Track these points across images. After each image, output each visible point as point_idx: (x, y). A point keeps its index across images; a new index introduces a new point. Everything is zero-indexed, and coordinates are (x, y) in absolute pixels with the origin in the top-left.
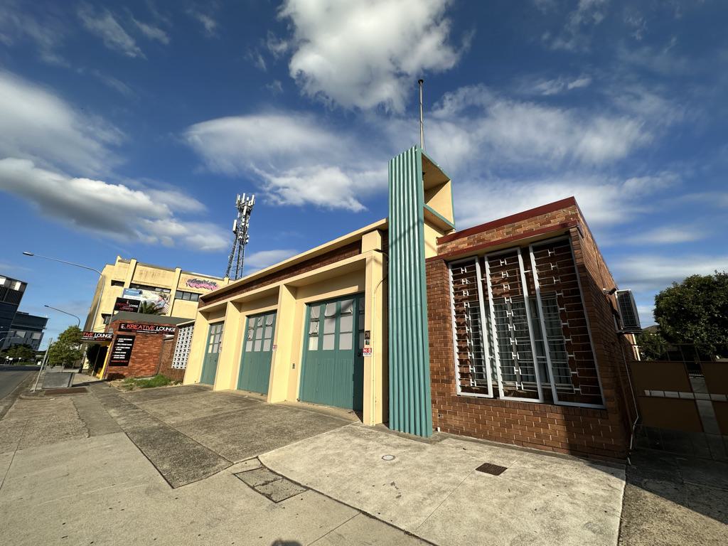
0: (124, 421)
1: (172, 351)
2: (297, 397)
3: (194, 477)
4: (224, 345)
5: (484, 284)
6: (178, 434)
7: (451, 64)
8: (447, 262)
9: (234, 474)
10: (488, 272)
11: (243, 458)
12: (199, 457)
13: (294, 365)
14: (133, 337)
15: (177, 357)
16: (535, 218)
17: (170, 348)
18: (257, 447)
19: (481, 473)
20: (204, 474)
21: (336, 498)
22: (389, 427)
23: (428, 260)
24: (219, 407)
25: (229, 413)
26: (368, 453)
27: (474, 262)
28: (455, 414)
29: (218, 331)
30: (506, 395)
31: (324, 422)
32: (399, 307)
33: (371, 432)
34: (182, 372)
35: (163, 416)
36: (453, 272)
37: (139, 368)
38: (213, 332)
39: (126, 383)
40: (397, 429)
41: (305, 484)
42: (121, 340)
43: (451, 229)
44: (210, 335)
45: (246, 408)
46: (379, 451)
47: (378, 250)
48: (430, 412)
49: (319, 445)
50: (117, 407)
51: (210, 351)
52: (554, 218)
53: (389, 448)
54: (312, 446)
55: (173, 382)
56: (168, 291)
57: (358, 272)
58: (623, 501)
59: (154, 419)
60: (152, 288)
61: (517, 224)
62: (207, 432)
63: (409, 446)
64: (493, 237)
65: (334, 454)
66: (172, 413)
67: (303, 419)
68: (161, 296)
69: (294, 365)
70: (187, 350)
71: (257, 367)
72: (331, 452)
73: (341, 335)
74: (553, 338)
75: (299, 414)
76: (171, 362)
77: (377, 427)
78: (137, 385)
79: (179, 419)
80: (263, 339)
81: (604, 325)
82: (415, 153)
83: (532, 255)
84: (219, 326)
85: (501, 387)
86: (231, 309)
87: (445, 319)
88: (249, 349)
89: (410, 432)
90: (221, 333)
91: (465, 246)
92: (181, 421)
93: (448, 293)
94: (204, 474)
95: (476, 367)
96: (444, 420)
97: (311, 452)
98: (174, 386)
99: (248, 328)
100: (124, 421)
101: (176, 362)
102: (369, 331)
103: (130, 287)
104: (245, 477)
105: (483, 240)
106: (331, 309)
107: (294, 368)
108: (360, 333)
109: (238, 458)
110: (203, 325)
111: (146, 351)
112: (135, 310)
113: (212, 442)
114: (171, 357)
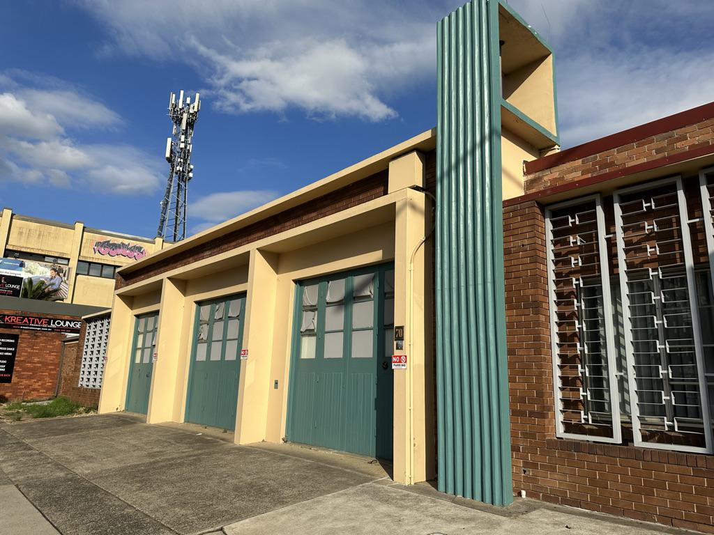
0: (12, 469)
1: (78, 359)
2: (283, 435)
5: (611, 244)
6: (95, 489)
8: (542, 207)
10: (619, 222)
13: (276, 383)
14: (16, 337)
17: (74, 356)
18: (222, 514)
24: (156, 450)
25: (173, 459)
27: (674, 188)
28: (553, 470)
29: (150, 328)
30: (645, 439)
31: (326, 478)
33: (408, 495)
34: (95, 395)
35: (70, 462)
36: (554, 224)
38: (141, 329)
39: (10, 409)
40: (450, 491)
43: (551, 147)
44: (137, 334)
47: (416, 188)
51: (138, 360)
54: (310, 514)
55: (81, 409)
56: (66, 262)
59: (58, 466)
61: (677, 133)
62: (140, 488)
64: (630, 158)
67: (294, 470)
68: (55, 270)
69: (276, 383)
70: (101, 359)
71: (216, 385)
73: (342, 328)
75: (287, 464)
77: (416, 488)
79: (96, 466)
80: (224, 340)
83: (617, 209)
84: (151, 320)
85: (636, 426)
86: (259, 267)
87: (538, 306)
90: (155, 330)
91: (577, 176)
96: (534, 479)
99: (199, 323)
101: (85, 377)
102: (402, 328)
105: (612, 164)
106: (336, 291)
107: (276, 387)
108: (387, 331)
113: (149, 504)
114: (77, 370)
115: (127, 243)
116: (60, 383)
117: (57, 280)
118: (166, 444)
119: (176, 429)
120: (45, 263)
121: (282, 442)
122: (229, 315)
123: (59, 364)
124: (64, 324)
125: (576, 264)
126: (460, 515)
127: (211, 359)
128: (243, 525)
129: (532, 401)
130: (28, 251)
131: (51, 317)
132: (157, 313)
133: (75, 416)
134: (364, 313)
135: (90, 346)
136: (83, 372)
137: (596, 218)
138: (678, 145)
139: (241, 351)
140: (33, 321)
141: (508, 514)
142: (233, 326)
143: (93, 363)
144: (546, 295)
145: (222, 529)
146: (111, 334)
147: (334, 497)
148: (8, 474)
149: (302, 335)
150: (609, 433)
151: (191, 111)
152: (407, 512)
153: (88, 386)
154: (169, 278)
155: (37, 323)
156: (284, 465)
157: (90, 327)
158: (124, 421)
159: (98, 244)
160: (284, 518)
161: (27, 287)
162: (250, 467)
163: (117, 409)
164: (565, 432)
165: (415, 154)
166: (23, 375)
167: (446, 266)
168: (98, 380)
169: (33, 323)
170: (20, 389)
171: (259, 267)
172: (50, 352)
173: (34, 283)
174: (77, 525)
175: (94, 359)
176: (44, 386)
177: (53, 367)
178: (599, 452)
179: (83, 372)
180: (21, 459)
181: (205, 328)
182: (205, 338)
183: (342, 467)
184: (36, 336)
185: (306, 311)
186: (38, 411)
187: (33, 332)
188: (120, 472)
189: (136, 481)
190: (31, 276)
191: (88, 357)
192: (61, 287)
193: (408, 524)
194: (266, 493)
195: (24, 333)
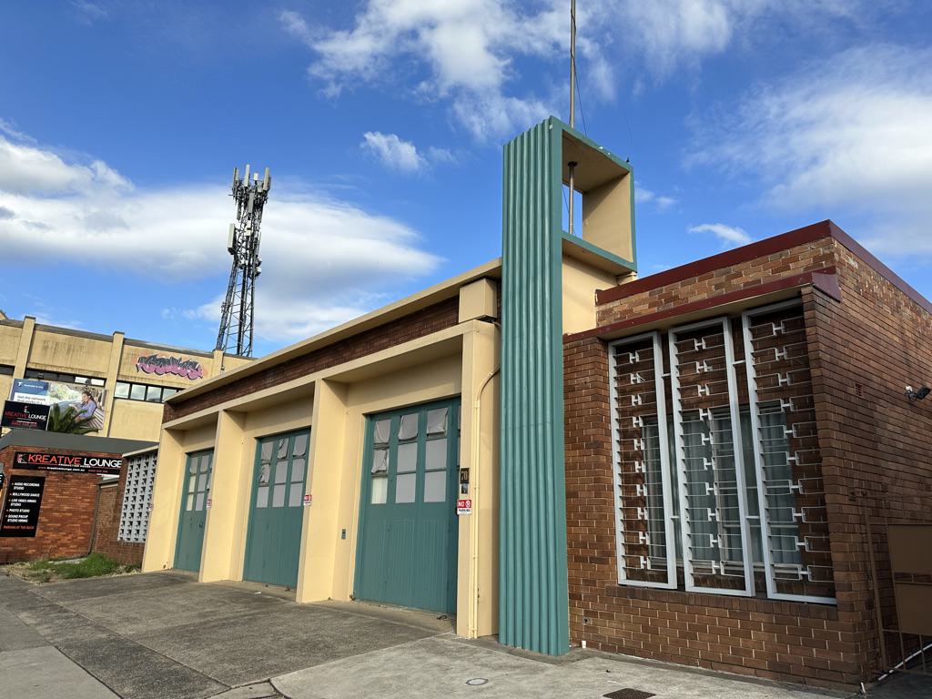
0: (49, 631)
1: (118, 507)
2: (351, 591)
4: (214, 495)
5: (741, 371)
6: (141, 649)
7: (416, 166)
8: (605, 342)
10: (674, 362)
12: (177, 680)
13: (344, 533)
14: (41, 480)
15: (127, 520)
16: (764, 257)
17: (112, 502)
22: (498, 641)
23: (567, 339)
24: (208, 610)
25: (226, 619)
27: (719, 329)
28: (611, 617)
29: (204, 469)
30: (698, 583)
31: (392, 632)
32: (517, 425)
33: (465, 648)
34: (138, 549)
36: (618, 360)
37: (54, 542)
38: (193, 470)
39: (34, 569)
40: (511, 644)
42: (19, 486)
43: (627, 273)
44: (188, 475)
45: (256, 611)
47: (485, 319)
48: (561, 614)
50: (30, 609)
52: (795, 259)
54: (360, 666)
55: (121, 568)
56: (101, 382)
57: (451, 354)
59: (98, 628)
60: (69, 378)
61: (733, 269)
62: (188, 647)
65: (391, 678)
66: (128, 619)
67: (355, 628)
68: (88, 394)
69: (344, 533)
70: (145, 506)
71: (276, 536)
72: (388, 675)
73: (415, 469)
74: (774, 484)
75: (350, 621)
76: (117, 529)
77: (480, 641)
78: (57, 573)
79: (141, 627)
80: (288, 483)
83: (673, 350)
84: (205, 458)
86: (325, 397)
87: (600, 447)
89: (531, 648)
90: (210, 470)
92: (144, 630)
93: (606, 399)
96: (594, 629)
98: (125, 574)
99: (259, 463)
100: (49, 631)
101: (126, 528)
102: (467, 470)
103: (25, 377)
105: (676, 298)
106: (409, 425)
107: (344, 537)
108: (457, 477)
109: (239, 680)
110: (172, 458)
112: (41, 425)
113: (197, 660)
114: (116, 519)
118: (219, 604)
120: (75, 385)
121: (349, 599)
123: (93, 513)
124: (101, 463)
126: (509, 664)
129: (593, 546)
130: (55, 370)
132: (211, 450)
133: (114, 576)
135: (132, 491)
136: (124, 522)
137: (653, 357)
138: (734, 282)
139: (305, 497)
140: (63, 460)
141: (553, 662)
142: (298, 464)
143: (136, 511)
144: (609, 434)
145: (269, 681)
146: (158, 477)
147: (390, 651)
148: (45, 636)
149: (373, 477)
150: (665, 579)
151: (259, 191)
152: (458, 662)
153: (129, 539)
154: (225, 410)
155: (67, 463)
156: (346, 622)
157: (132, 467)
160: (333, 671)
161: (53, 416)
162: (310, 625)
164: (627, 578)
165: (484, 281)
166: (50, 527)
168: (142, 532)
169: (63, 462)
170: (45, 544)
171: (325, 397)
172: (83, 498)
173: (62, 411)
176: (75, 540)
177: (86, 517)
178: (651, 598)
180: (57, 621)
181: (267, 468)
182: (267, 481)
184: (66, 478)
185: (378, 449)
186: (68, 572)
187: (63, 473)
188: (168, 632)
189: (185, 642)
190: (57, 401)
191: (129, 503)
193: (454, 672)
195: (51, 475)
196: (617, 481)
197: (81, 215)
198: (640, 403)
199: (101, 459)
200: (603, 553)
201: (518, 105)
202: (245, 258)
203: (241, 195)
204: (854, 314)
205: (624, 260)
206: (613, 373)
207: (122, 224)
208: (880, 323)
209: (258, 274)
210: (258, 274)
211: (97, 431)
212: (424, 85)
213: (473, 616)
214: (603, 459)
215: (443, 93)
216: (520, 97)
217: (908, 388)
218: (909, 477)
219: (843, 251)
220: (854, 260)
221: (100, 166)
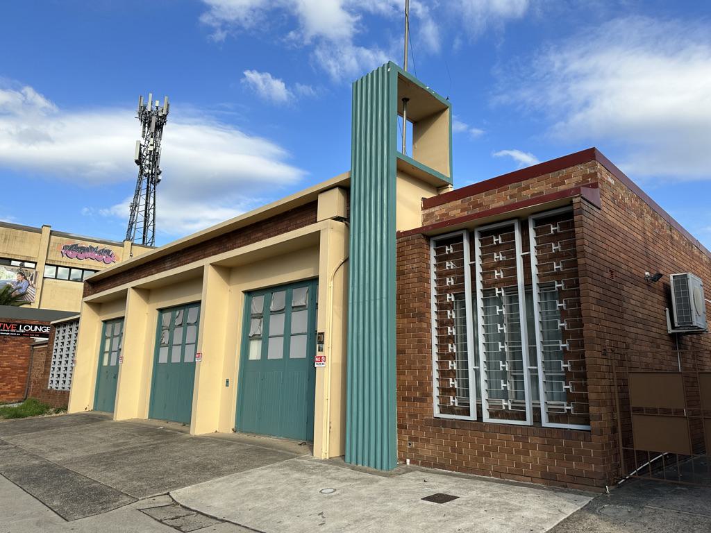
1: (47, 363)
2: (233, 426)
3: (91, 512)
4: (125, 353)
6: (67, 471)
8: (428, 238)
9: (140, 510)
11: (151, 494)
13: (227, 382)
15: (55, 373)
18: (170, 484)
19: (425, 501)
20: (102, 509)
21: (253, 528)
25: (135, 448)
26: (306, 486)
27: (512, 228)
28: (428, 441)
29: (116, 333)
30: (492, 415)
34: (64, 396)
35: (43, 453)
36: (437, 251)
38: (108, 334)
41: (222, 518)
43: (445, 185)
44: (104, 338)
45: (159, 442)
46: (321, 484)
47: (338, 219)
49: (249, 480)
52: (569, 177)
53: (334, 482)
54: (239, 481)
55: (51, 410)
56: (33, 265)
57: (311, 246)
58: (561, 522)
59: (33, 456)
61: (524, 183)
62: (105, 470)
63: (360, 479)
64: (493, 201)
65: (263, 490)
66: (56, 449)
68: (22, 274)
69: (227, 382)
70: (70, 362)
71: (174, 384)
72: (260, 487)
73: (283, 333)
77: (331, 461)
79: (67, 455)
80: (184, 345)
81: (618, 326)
82: (388, 73)
84: (118, 325)
85: (485, 406)
87: (423, 316)
88: (163, 358)
89: (369, 465)
90: (121, 335)
91: (457, 213)
92: (70, 458)
93: (428, 280)
94: (102, 509)
95: (572, 384)
97: (236, 488)
98: (54, 415)
101: (55, 379)
102: (323, 334)
104: (153, 512)
105: (480, 205)
106: (278, 300)
108: (315, 339)
110: (91, 324)
111: (6, 364)
113: (112, 480)
114: (46, 373)
115: (95, 247)
116: (29, 386)
117: (24, 284)
118: (130, 437)
119: (140, 424)
120: (11, 267)
121: (231, 432)
122: (293, 305)
124: (33, 329)
125: (450, 283)
127: (172, 362)
128: (186, 490)
129: (416, 389)
131: (20, 322)
134: (299, 321)
135: (59, 350)
136: (54, 368)
138: (524, 193)
139: (197, 355)
143: (62, 373)
144: (429, 306)
149: (251, 340)
151: (160, 114)
153: (57, 388)
154: (133, 288)
155: (6, 329)
156: (229, 449)
157: (59, 331)
158: (93, 419)
159: (65, 248)
162: (200, 451)
163: (86, 409)
164: (441, 413)
165: (337, 189)
167: (356, 284)
172: (19, 356)
174: (53, 495)
175: (63, 362)
179: (54, 368)
183: (276, 448)
185: (254, 318)
186: (8, 413)
191: (57, 360)
192: (29, 290)
193: (311, 484)
194: (208, 469)
196: (435, 341)
197: (14, 131)
198: (452, 284)
199: (34, 326)
200: (423, 394)
201: (366, 53)
202: (149, 168)
203: (145, 118)
204: (610, 218)
205: (444, 176)
206: (433, 261)
207: (48, 139)
208: (629, 225)
209: (159, 181)
210: (159, 181)
211: (30, 303)
212: (292, 34)
213: (326, 442)
214: (425, 325)
215: (307, 42)
216: (367, 47)
217: (647, 273)
218: (647, 338)
219: (604, 172)
220: (612, 178)
221: (29, 91)
